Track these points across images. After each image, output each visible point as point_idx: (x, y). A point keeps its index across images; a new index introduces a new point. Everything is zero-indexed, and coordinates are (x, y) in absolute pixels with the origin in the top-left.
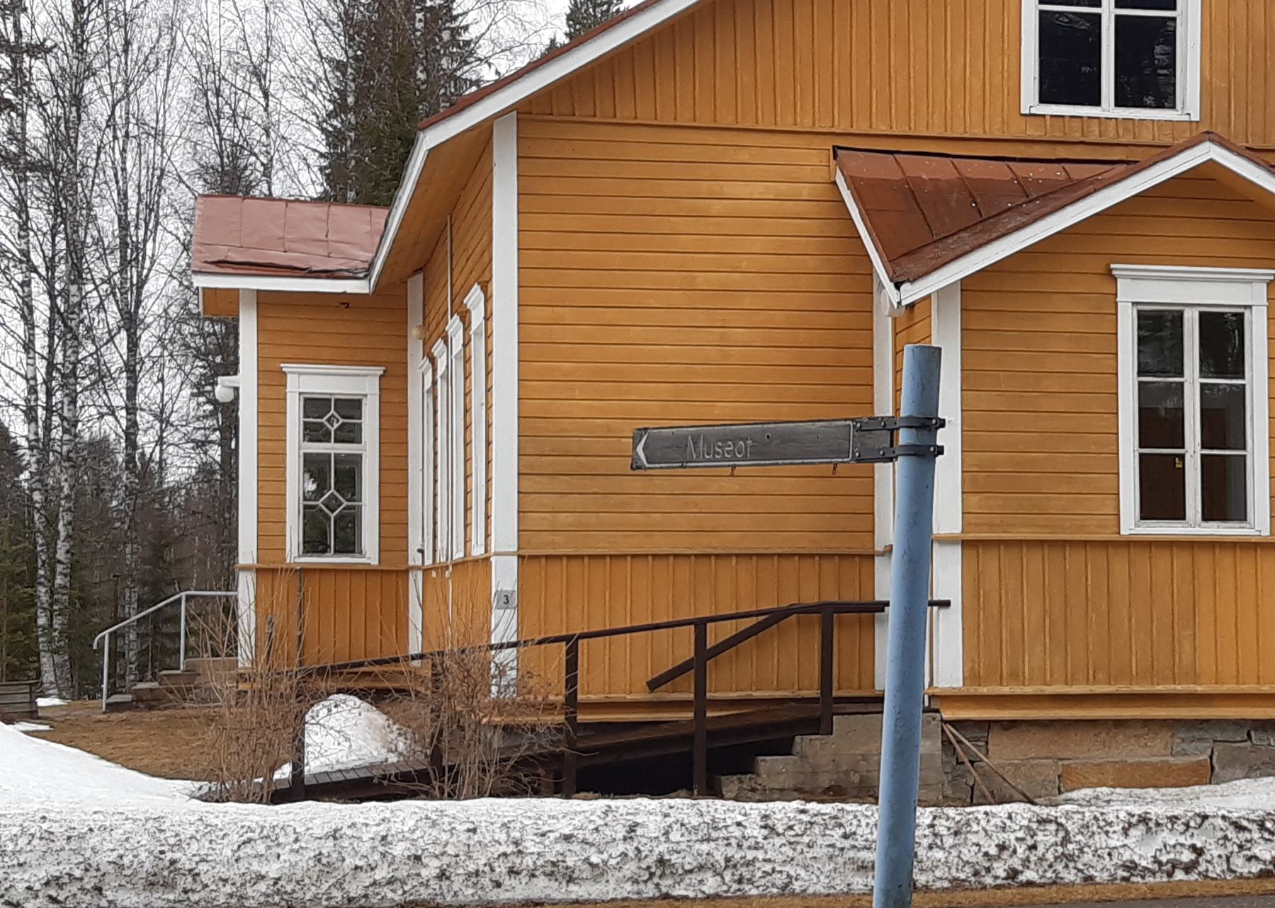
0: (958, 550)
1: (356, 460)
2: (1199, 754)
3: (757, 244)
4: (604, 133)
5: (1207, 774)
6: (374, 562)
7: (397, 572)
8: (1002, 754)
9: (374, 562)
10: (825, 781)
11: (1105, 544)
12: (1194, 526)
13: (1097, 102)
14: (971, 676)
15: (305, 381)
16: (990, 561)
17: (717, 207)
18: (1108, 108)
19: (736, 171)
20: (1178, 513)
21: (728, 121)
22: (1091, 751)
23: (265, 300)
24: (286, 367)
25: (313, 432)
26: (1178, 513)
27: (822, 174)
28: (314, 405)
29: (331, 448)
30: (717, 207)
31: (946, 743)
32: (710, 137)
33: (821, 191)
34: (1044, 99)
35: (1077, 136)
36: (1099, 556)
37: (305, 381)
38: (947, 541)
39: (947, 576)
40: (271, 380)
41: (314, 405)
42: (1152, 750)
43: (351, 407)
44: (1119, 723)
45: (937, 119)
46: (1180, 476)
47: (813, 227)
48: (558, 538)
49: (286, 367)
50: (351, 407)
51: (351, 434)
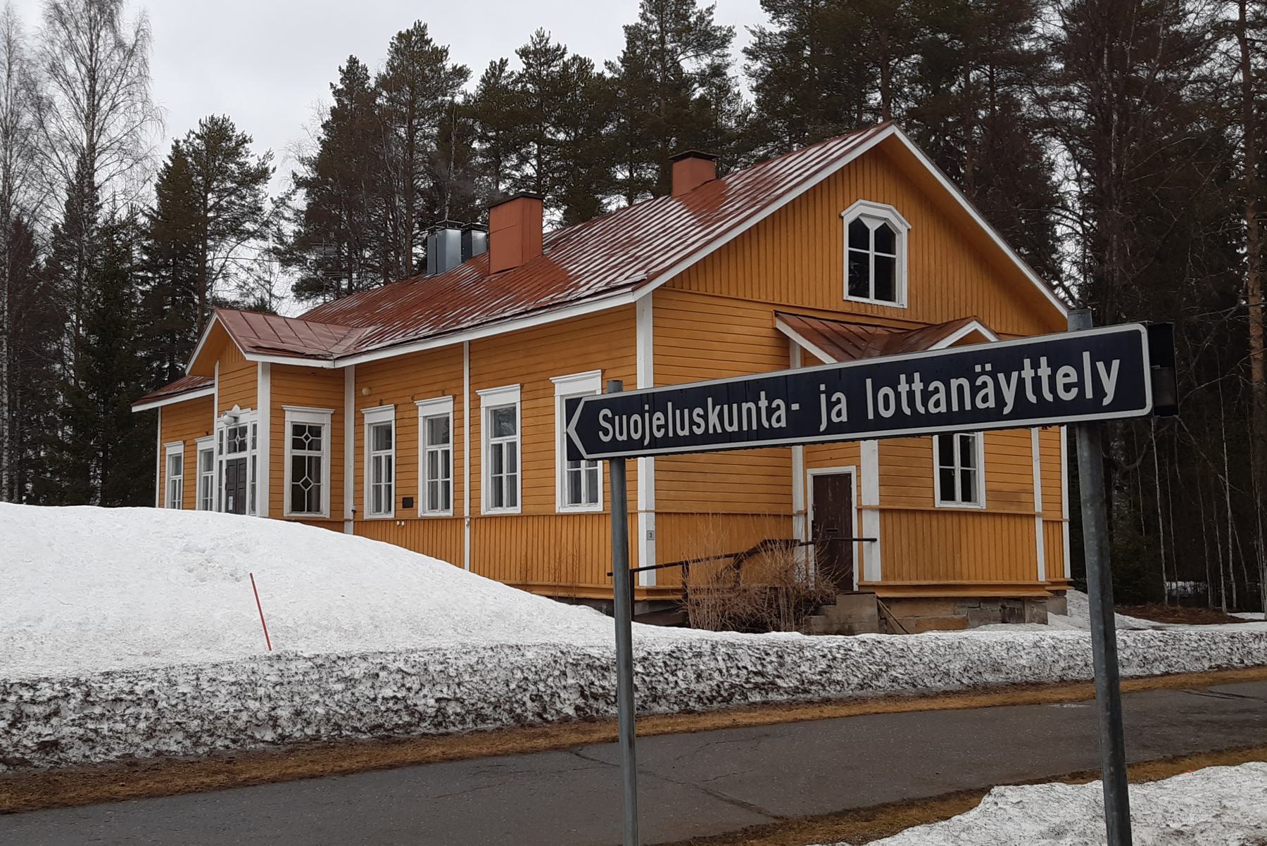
0: (877, 514)
1: (318, 459)
2: (963, 613)
3: (746, 357)
4: (695, 298)
5: (963, 625)
6: (328, 516)
7: (1028, 516)
8: (896, 613)
9: (328, 516)
10: (835, 628)
11: (930, 512)
12: (958, 504)
13: (868, 297)
14: (885, 576)
15: (295, 416)
16: (888, 516)
17: (730, 338)
18: (871, 300)
19: (737, 320)
20: (952, 498)
21: (741, 296)
22: (927, 612)
23: (275, 370)
24: (286, 407)
25: (297, 444)
26: (952, 498)
27: (770, 324)
28: (298, 429)
29: (305, 453)
30: (730, 338)
31: (879, 609)
32: (735, 303)
33: (770, 332)
34: (850, 294)
35: (863, 312)
36: (926, 516)
37: (295, 416)
38: (872, 509)
39: (869, 525)
40: (277, 414)
41: (298, 429)
42: (945, 612)
43: (316, 431)
44: (937, 599)
45: (812, 300)
46: (953, 478)
47: (767, 350)
48: (670, 503)
49: (286, 407)
50: (316, 431)
51: (316, 446)
